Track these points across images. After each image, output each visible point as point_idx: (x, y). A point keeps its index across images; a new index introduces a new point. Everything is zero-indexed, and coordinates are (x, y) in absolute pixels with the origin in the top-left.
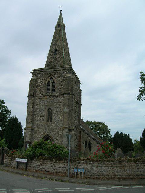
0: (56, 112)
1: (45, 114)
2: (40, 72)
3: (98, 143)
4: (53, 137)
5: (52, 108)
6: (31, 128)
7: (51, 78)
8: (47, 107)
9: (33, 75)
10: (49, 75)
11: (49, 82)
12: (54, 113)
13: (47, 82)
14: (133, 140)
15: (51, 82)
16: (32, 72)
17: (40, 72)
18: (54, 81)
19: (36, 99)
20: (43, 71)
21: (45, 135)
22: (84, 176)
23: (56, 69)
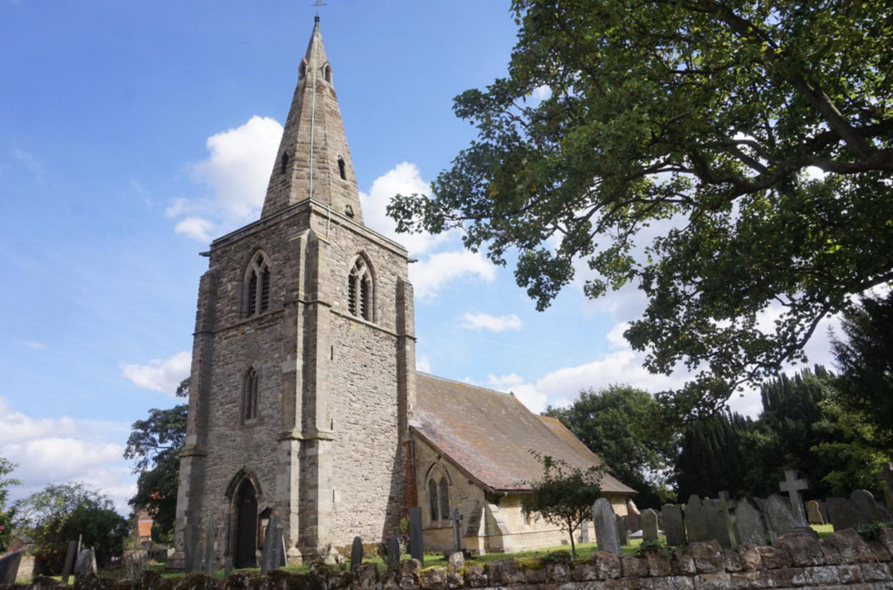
0: (269, 377)
1: (239, 392)
2: (227, 246)
3: (471, 483)
4: (259, 475)
5: (257, 365)
6: (192, 452)
7: (260, 261)
8: (243, 366)
9: (210, 260)
10: (250, 250)
11: (253, 273)
12: (263, 384)
13: (248, 274)
14: (642, 319)
15: (258, 271)
16: (208, 249)
17: (227, 246)
18: (266, 268)
19: (215, 345)
20: (236, 238)
21: (237, 471)
22: (842, 112)
23: (269, 224)
